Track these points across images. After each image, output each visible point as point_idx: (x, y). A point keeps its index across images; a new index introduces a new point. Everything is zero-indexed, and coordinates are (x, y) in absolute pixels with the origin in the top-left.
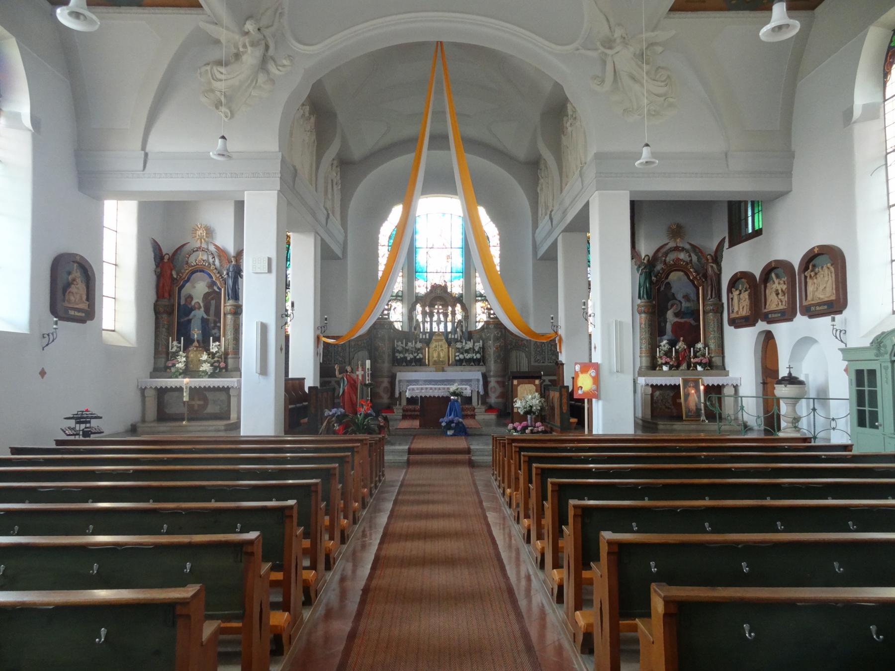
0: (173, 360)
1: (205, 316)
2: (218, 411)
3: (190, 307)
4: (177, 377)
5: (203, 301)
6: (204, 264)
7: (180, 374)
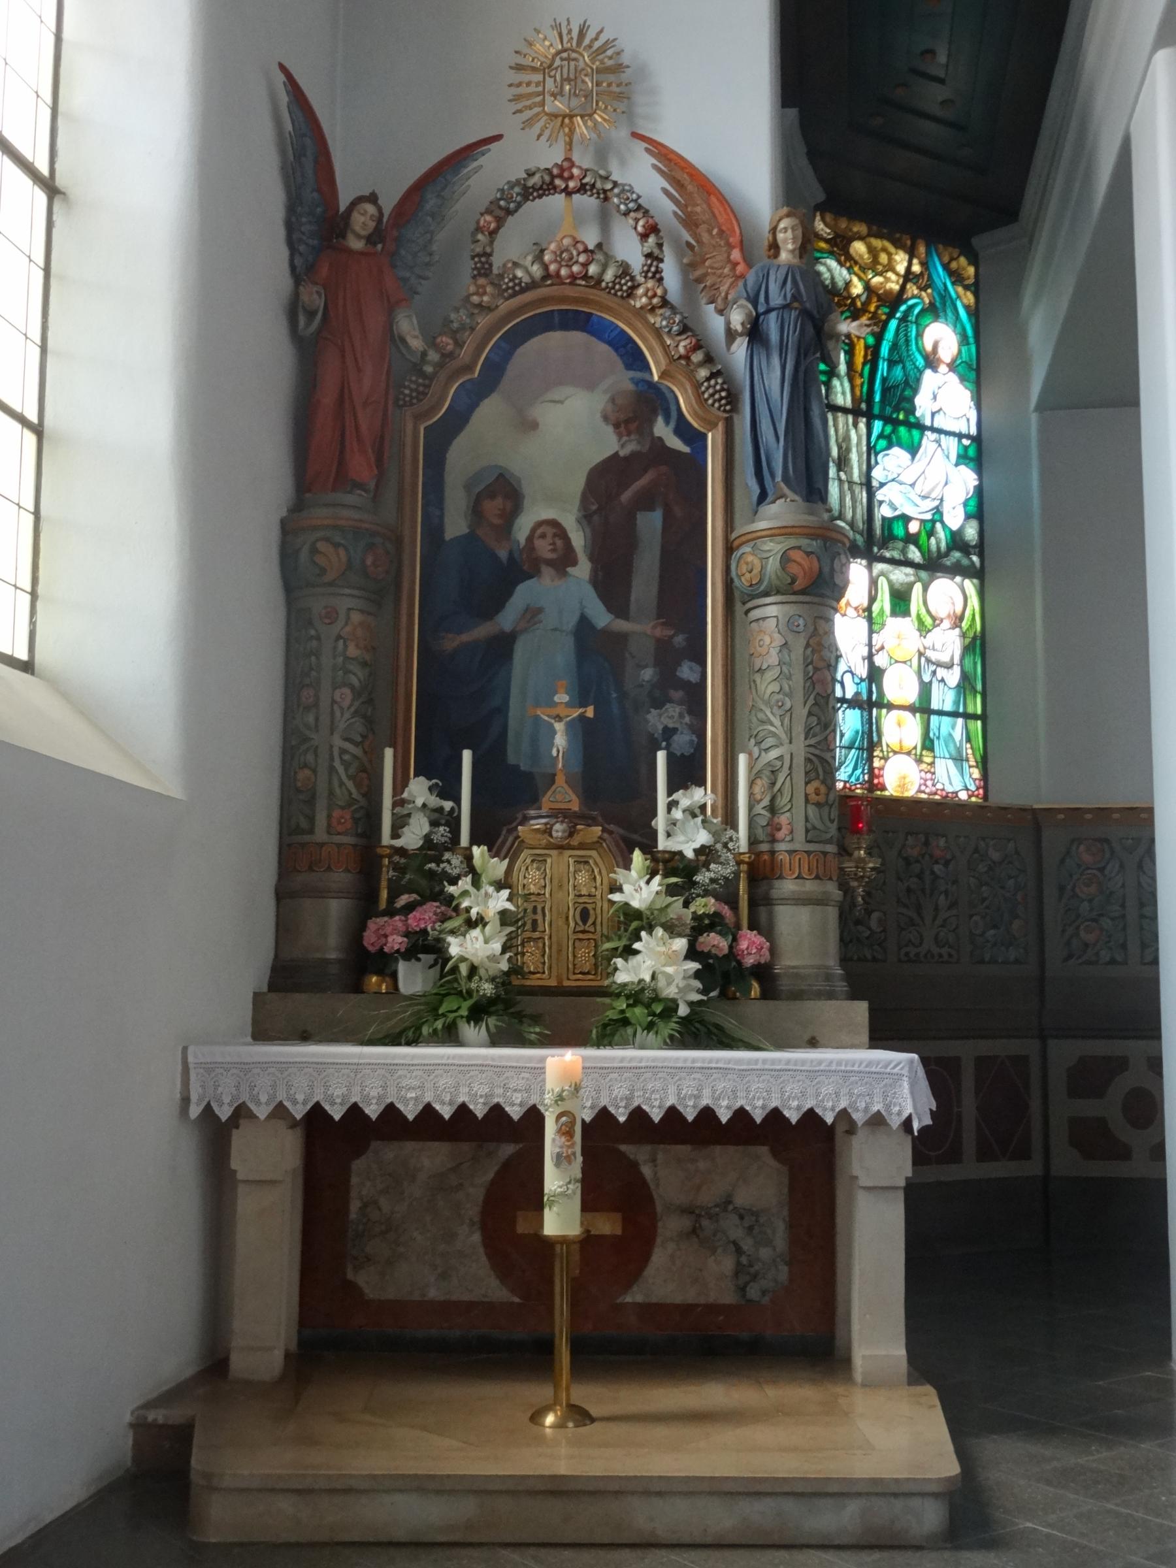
0: (410, 908)
1: (602, 618)
2: (723, 1294)
3: (503, 554)
4: (450, 1036)
5: (586, 517)
6: (593, 269)
7: (477, 1014)
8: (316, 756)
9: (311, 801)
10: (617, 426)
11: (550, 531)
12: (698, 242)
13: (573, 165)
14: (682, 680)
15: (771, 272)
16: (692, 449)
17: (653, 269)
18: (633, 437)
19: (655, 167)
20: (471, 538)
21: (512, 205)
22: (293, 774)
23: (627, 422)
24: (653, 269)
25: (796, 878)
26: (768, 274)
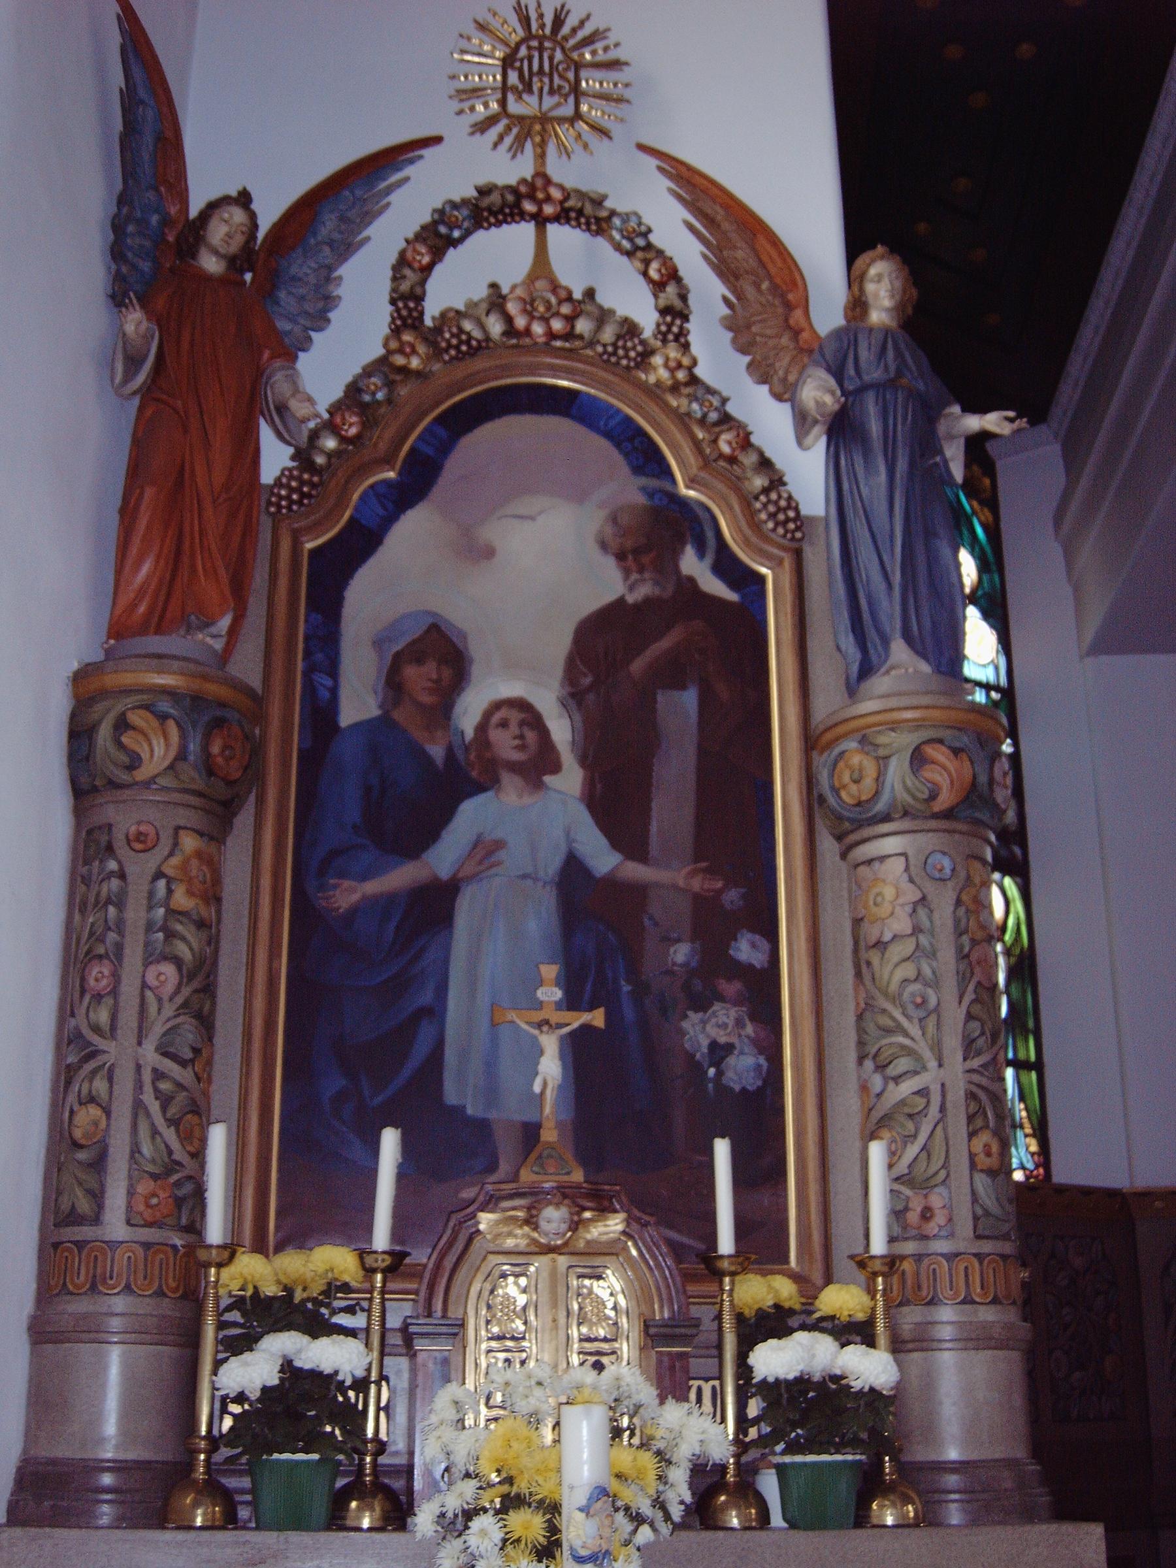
3: (437, 752)
8: (110, 1079)
9: (99, 1164)
10: (620, 557)
11: (515, 716)
12: (739, 299)
13: (548, 181)
14: (737, 963)
15: (860, 336)
16: (743, 597)
17: (675, 329)
18: (647, 575)
19: (670, 190)
20: (382, 725)
21: (456, 234)
22: (67, 1114)
23: (637, 552)
24: (675, 329)
25: (959, 1303)
26: (856, 341)
